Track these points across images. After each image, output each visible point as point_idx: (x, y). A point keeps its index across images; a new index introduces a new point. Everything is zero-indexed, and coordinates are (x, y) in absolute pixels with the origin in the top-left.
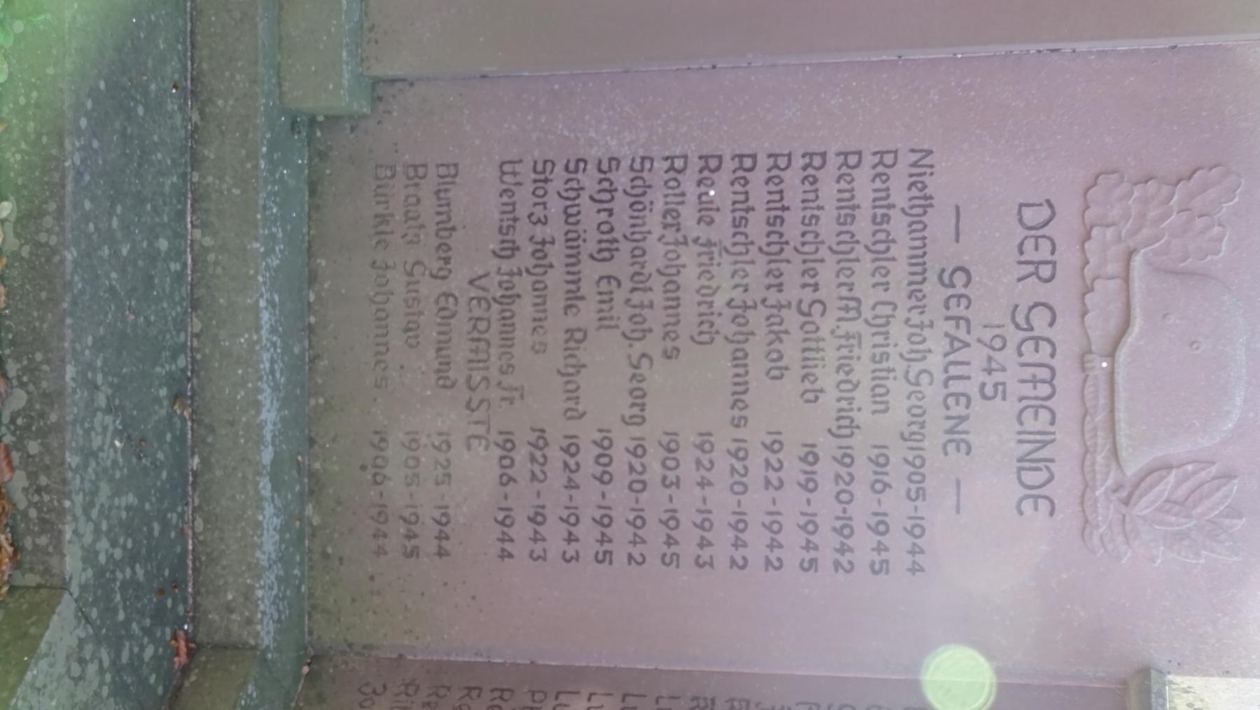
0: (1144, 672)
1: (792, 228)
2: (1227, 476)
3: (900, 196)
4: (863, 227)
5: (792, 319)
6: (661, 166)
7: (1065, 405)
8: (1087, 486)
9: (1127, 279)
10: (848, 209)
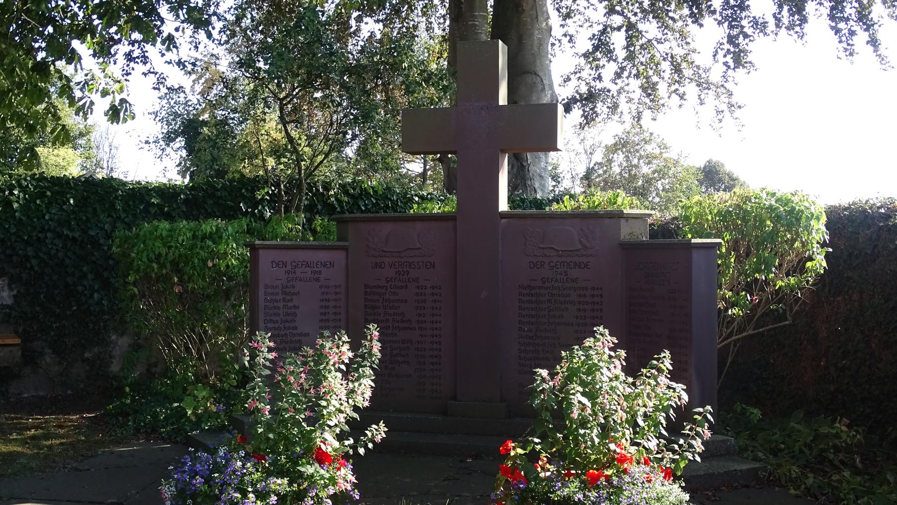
0: (621, 245)
1: (534, 313)
2: (582, 229)
3: (528, 291)
4: (534, 299)
5: (552, 313)
6: (520, 340)
7: (568, 260)
8: (584, 255)
9: (543, 248)
10: (531, 302)
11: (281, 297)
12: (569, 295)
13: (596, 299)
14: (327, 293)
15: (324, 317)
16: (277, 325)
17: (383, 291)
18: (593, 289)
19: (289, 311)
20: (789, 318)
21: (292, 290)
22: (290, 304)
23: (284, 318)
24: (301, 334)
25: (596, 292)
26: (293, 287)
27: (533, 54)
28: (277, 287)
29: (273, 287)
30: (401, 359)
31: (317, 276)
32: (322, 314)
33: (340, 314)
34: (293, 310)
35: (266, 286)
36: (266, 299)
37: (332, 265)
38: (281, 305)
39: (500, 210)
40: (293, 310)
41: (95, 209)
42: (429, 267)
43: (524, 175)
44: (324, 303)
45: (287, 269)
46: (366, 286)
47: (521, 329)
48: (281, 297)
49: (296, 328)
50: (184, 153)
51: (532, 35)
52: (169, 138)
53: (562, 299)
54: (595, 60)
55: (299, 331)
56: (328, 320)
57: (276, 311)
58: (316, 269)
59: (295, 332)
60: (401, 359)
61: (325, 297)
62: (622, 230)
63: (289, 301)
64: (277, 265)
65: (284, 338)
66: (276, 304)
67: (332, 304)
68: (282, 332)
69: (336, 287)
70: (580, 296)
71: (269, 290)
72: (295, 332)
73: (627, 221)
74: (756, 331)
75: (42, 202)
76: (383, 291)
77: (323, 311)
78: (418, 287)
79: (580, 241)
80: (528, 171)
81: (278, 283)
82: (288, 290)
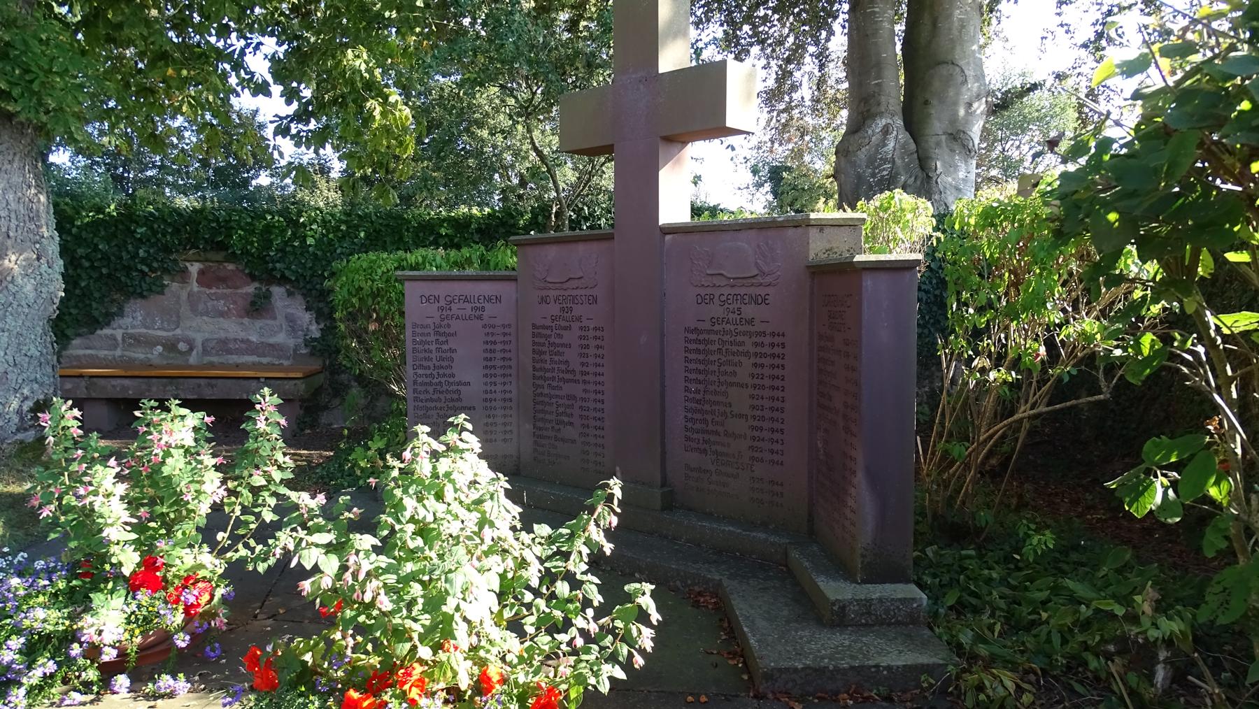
1: (701, 367)
4: (701, 347)
5: (722, 368)
7: (742, 291)
11: (433, 338)
12: (742, 344)
13: (777, 350)
14: (493, 334)
15: (489, 364)
16: (428, 372)
17: (548, 332)
18: (773, 334)
19: (444, 355)
20: (1105, 389)
21: (447, 330)
22: (445, 347)
23: (437, 364)
24: (459, 383)
25: (777, 340)
26: (449, 326)
27: (952, 39)
28: (427, 326)
29: (422, 326)
30: (566, 419)
31: (478, 313)
32: (486, 359)
33: (510, 359)
34: (448, 354)
35: (415, 325)
36: (414, 341)
37: (498, 299)
38: (433, 347)
39: (661, 223)
40: (448, 354)
41: (385, 242)
42: (746, 301)
43: (930, 188)
44: (489, 347)
45: (440, 305)
46: (534, 326)
47: (687, 390)
48: (433, 338)
49: (453, 376)
50: (770, 197)
51: (950, 16)
52: (759, 185)
53: (735, 348)
54: (1098, 49)
55: (457, 379)
56: (494, 367)
57: (427, 355)
58: (478, 305)
59: (451, 380)
60: (566, 419)
61: (490, 338)
62: (812, 246)
63: (442, 343)
64: (428, 300)
65: (438, 387)
66: (427, 347)
67: (499, 347)
68: (435, 381)
69: (504, 326)
70: (756, 344)
71: (418, 330)
72: (451, 380)
73: (821, 230)
74: (1050, 408)
75: (335, 236)
76: (548, 332)
77: (488, 355)
78: (581, 328)
79: (756, 263)
80: (937, 183)
81: (429, 321)
82: (442, 330)
